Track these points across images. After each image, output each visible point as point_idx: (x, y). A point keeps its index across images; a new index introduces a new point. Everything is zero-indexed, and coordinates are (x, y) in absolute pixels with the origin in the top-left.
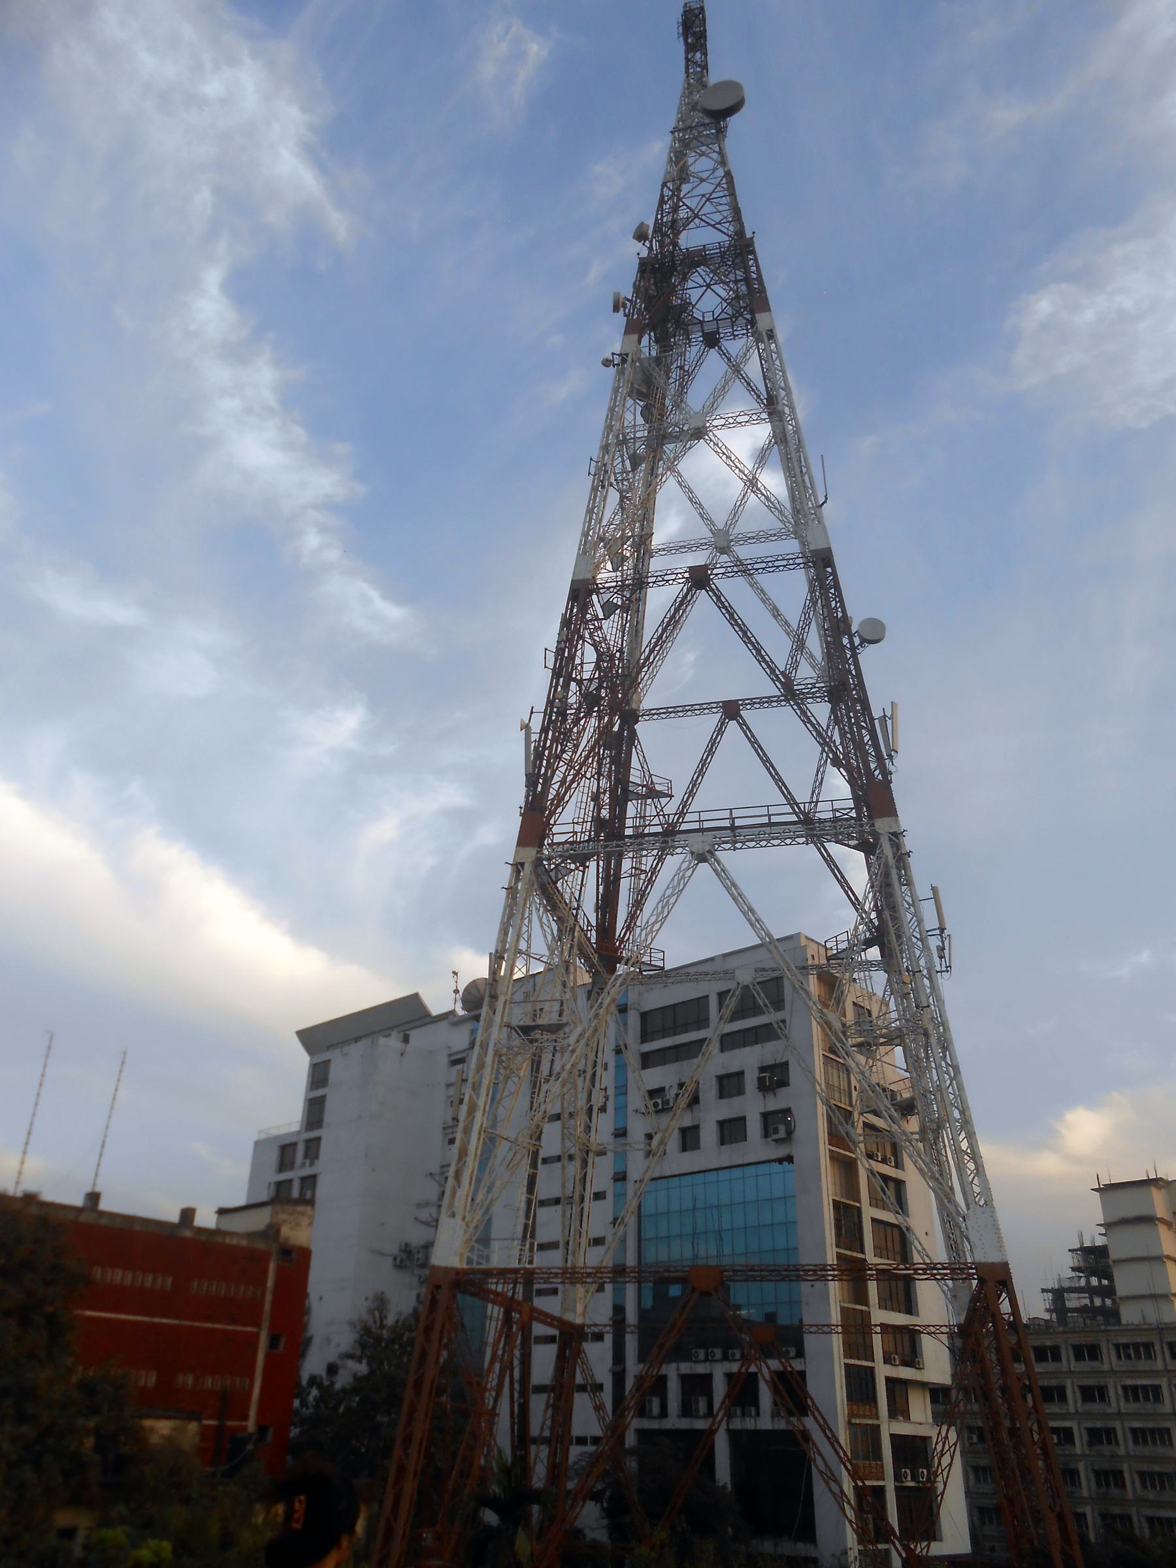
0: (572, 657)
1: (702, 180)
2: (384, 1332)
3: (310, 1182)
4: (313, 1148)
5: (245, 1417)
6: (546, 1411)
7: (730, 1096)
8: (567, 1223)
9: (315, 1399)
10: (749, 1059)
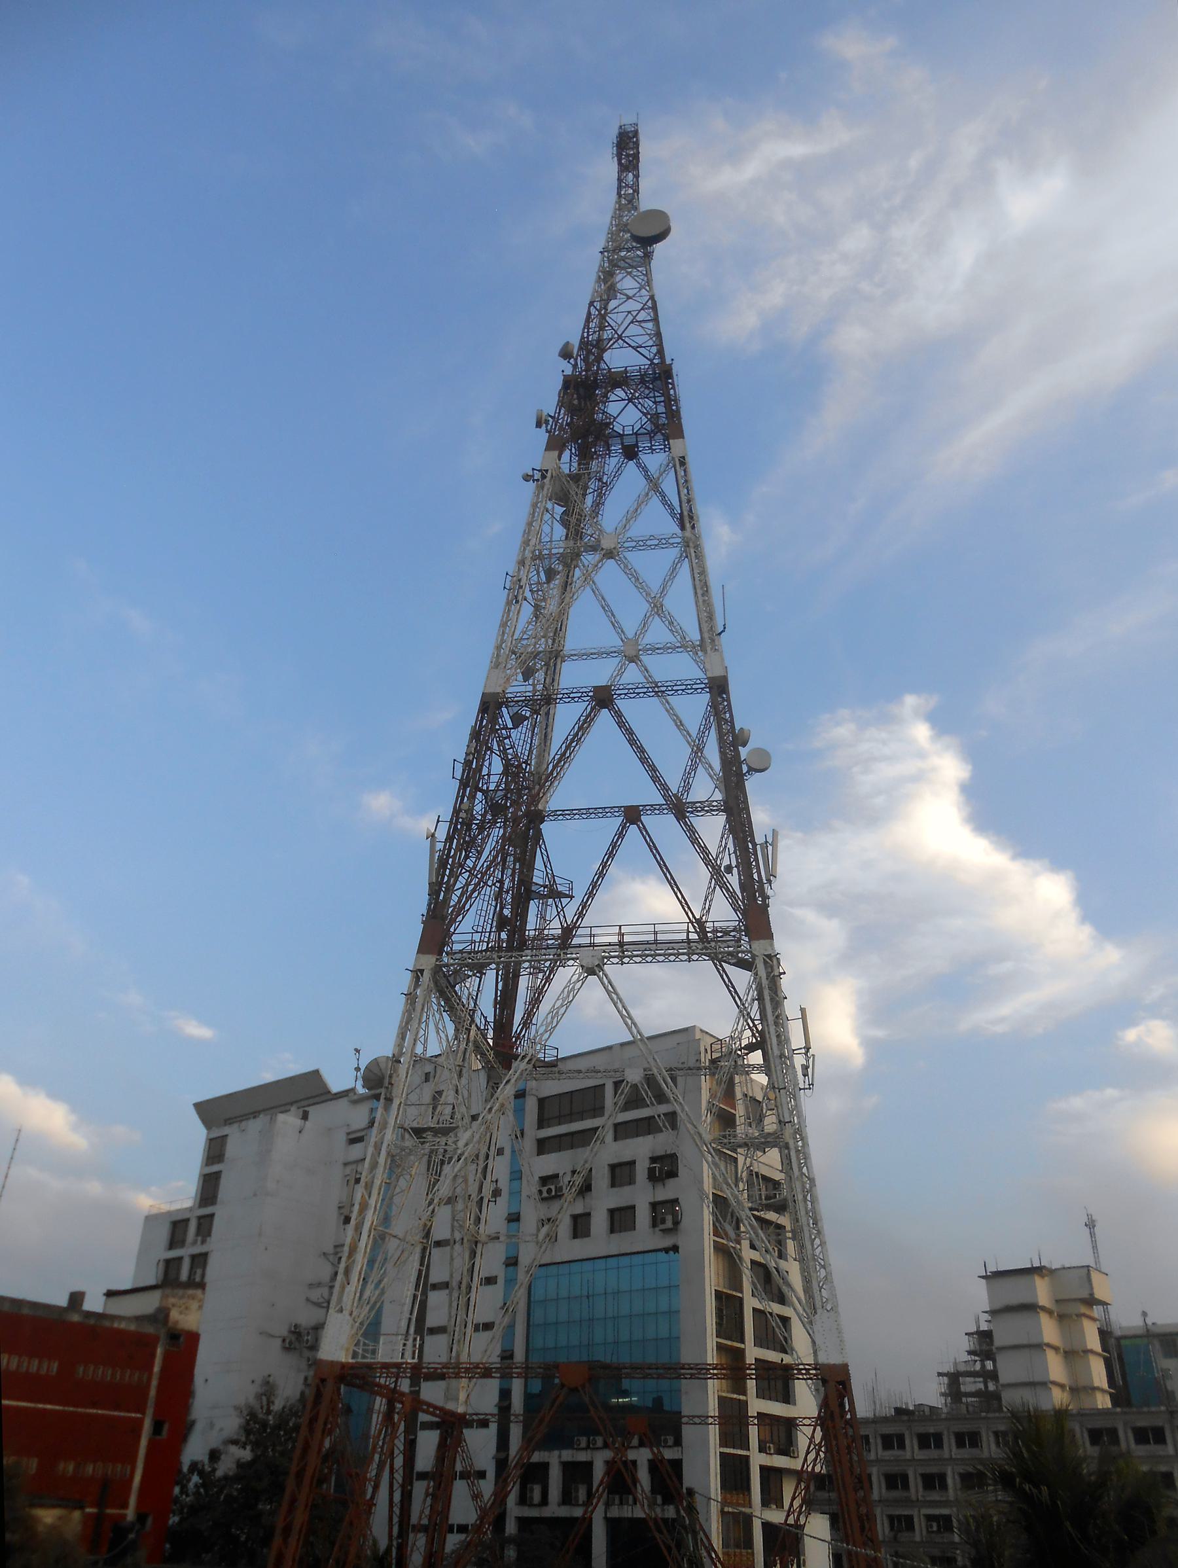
0: (479, 769)
1: (629, 298)
2: (270, 1417)
3: (200, 1260)
4: (205, 1225)
5: (125, 1505)
6: (425, 1500)
7: (621, 1185)
8: (454, 1312)
9: (196, 1485)
10: (641, 1149)
